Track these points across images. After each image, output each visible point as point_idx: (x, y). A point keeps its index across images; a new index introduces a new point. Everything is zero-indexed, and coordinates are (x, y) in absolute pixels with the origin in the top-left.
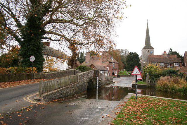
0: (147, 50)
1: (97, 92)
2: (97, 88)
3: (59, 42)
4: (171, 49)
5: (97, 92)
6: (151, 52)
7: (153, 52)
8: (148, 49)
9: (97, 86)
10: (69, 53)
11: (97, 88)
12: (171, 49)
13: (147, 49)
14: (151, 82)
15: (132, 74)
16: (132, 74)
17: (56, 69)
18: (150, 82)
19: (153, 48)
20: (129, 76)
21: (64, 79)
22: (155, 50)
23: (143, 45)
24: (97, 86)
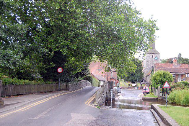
4: (180, 55)
6: (156, 58)
12: (180, 55)
18: (161, 95)
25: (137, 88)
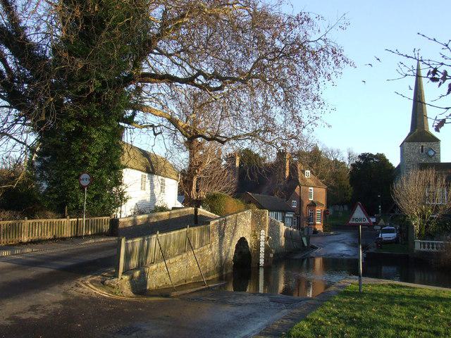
0: (417, 146)
1: (261, 272)
2: (262, 261)
3: (153, 130)
4: (353, 65)
5: (261, 272)
6: (431, 153)
7: (437, 153)
8: (422, 144)
9: (262, 255)
10: (181, 159)
11: (262, 261)
12: (353, 65)
15: (350, 222)
16: (350, 222)
17: (178, 280)
21: (181, 210)
22: (442, 145)
23: (405, 129)
24: (262, 255)
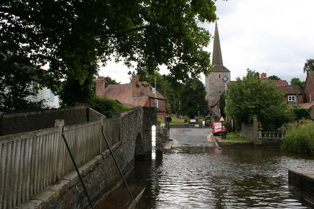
6: (225, 79)
13: (216, 73)
14: (263, 135)
19: (229, 71)
20: (185, 125)
25: (198, 126)
